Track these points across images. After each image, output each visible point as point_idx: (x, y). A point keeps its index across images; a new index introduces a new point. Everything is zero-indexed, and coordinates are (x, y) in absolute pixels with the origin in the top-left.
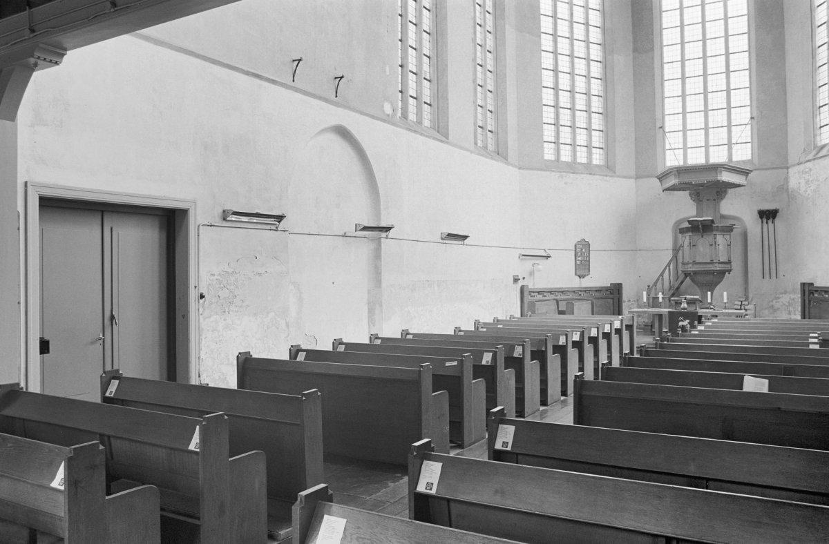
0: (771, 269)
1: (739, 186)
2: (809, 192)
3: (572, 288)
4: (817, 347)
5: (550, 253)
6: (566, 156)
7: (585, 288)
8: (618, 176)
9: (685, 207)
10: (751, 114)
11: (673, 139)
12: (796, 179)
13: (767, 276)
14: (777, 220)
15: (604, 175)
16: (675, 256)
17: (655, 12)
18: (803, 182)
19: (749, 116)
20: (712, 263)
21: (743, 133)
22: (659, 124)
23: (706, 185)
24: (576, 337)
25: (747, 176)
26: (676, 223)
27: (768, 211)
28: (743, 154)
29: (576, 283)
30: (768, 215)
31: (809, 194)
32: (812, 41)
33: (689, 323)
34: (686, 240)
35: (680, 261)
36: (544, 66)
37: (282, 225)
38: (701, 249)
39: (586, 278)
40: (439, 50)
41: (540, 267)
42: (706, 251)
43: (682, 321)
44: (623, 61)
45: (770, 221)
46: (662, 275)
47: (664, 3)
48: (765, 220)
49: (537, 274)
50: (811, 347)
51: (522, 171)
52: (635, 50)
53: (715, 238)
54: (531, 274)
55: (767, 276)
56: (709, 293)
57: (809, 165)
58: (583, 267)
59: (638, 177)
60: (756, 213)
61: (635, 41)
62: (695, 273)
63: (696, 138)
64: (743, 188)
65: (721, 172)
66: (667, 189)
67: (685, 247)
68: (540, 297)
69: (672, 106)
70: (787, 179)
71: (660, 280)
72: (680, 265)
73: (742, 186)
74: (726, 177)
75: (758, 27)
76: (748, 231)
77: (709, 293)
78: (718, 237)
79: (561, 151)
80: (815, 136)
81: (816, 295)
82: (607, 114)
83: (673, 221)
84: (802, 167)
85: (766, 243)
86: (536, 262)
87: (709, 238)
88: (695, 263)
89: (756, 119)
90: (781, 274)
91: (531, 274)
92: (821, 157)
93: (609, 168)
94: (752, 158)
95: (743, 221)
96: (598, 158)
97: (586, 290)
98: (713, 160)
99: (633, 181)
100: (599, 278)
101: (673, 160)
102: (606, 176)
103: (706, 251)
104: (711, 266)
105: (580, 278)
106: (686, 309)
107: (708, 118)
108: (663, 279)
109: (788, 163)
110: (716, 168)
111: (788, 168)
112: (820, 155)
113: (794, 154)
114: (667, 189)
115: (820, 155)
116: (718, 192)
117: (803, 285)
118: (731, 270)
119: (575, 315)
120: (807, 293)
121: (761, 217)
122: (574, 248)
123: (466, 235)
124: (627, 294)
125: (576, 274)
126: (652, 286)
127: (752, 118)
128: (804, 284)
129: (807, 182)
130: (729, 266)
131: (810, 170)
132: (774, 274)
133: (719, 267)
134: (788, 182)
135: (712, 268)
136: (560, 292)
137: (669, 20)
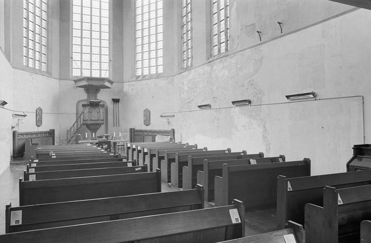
0: (117, 123)
1: (109, 88)
2: (133, 92)
3: (31, 132)
4: (55, 157)
5: (26, 114)
6: (153, 71)
7: (41, 132)
8: (53, 78)
9: (83, 95)
10: (109, 59)
11: (76, 64)
12: (127, 87)
13: (115, 126)
15: (48, 77)
17: (71, 5)
18: (130, 89)
20: (98, 120)
21: (105, 66)
22: (71, 56)
23: (93, 87)
24: (146, 150)
25: (112, 84)
26: (78, 101)
27: (116, 99)
28: (105, 75)
29: (36, 129)
30: (116, 101)
31: (133, 94)
33: (107, 146)
34: (87, 110)
38: (94, 114)
39: (41, 126)
41: (23, 121)
42: (96, 115)
43: (104, 145)
44: (56, 23)
45: (117, 104)
46: (74, 125)
47: (74, 2)
48: (115, 103)
49: (20, 124)
50: (53, 157)
51: (14, 69)
53: (100, 110)
54: (18, 125)
55: (115, 126)
56: (94, 134)
57: (133, 83)
58: (39, 122)
59: (60, 79)
60: (111, 100)
62: (91, 124)
63: (86, 65)
64: (108, 89)
68: (22, 137)
69: (76, 49)
70: (123, 87)
71: (73, 128)
73: (77, 87)
75: (114, 24)
77: (94, 134)
78: (101, 109)
80: (135, 72)
81: (136, 133)
82: (47, 47)
83: (77, 101)
84: (130, 83)
85: (115, 112)
86: (20, 118)
87: (97, 109)
88: (91, 120)
89: (112, 61)
90: (120, 125)
91: (18, 125)
93: (49, 73)
95: (105, 102)
96: (44, 68)
97: (41, 133)
98: (103, 76)
99: (58, 81)
100: (45, 127)
101: (76, 73)
102: (49, 77)
103: (96, 115)
104: (98, 121)
105: (38, 126)
106: (105, 140)
107: (91, 58)
109: (123, 81)
110: (103, 80)
111: (123, 83)
113: (126, 77)
115: (138, 80)
116: (96, 90)
117: (131, 129)
119: (56, 145)
120: (133, 132)
122: (35, 112)
123: (7, 102)
124: (56, 134)
125: (36, 125)
126: (69, 131)
128: (131, 129)
129: (132, 89)
131: (134, 85)
134: (123, 88)
135: (98, 122)
136: (25, 134)
137: (76, 10)
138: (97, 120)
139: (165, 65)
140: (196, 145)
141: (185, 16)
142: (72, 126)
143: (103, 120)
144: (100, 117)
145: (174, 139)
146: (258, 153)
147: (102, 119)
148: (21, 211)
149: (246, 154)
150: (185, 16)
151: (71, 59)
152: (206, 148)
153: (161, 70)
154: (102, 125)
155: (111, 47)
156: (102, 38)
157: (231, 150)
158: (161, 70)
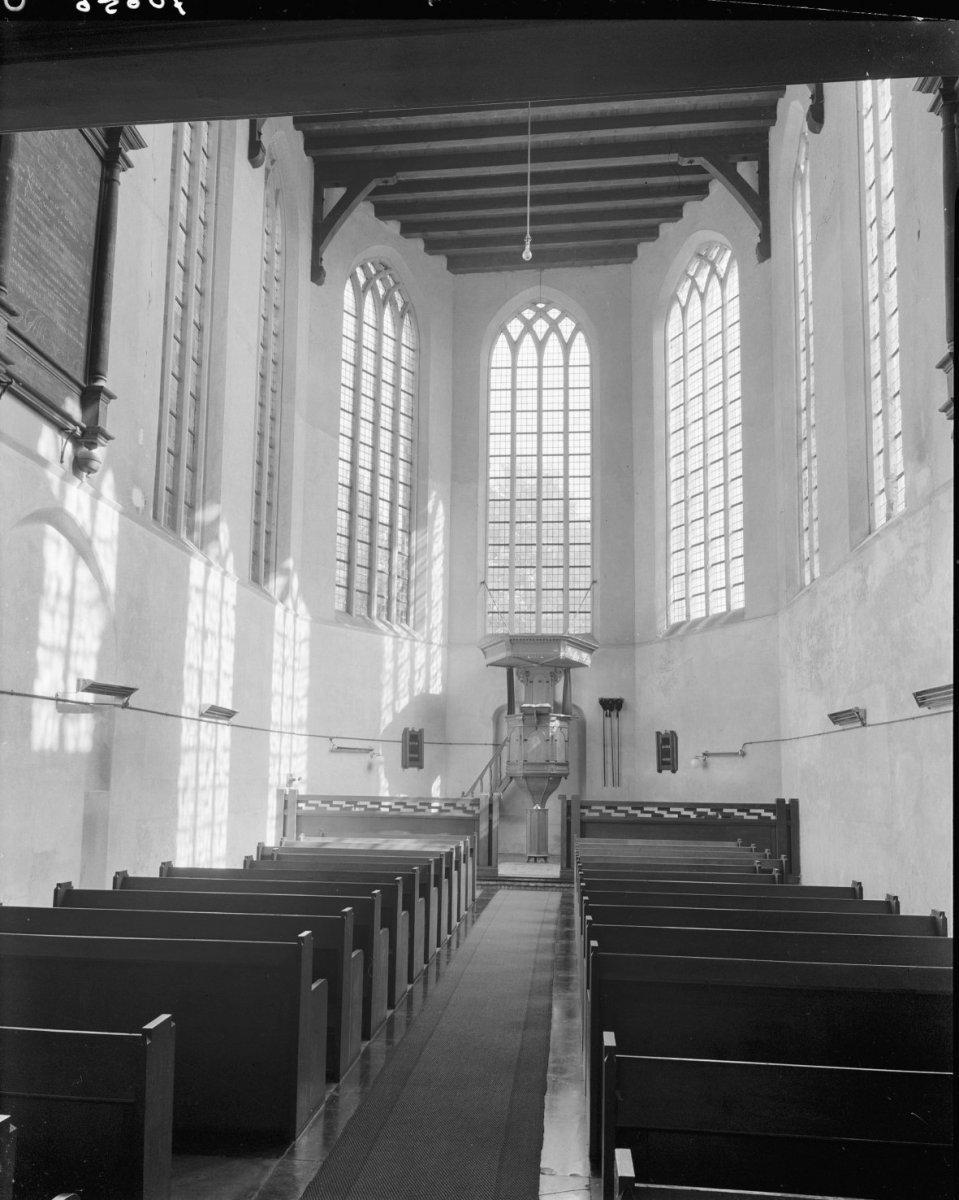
6: (718, 606)
14: (621, 713)
16: (497, 756)
19: (589, 579)
28: (579, 625)
30: (612, 706)
32: (861, 245)
35: (505, 760)
36: (341, 430)
37: (133, 700)
40: (210, 425)
45: (614, 713)
46: (481, 778)
52: (454, 478)
60: (597, 702)
61: (454, 467)
65: (565, 646)
66: (492, 664)
67: (513, 740)
72: (504, 765)
74: (571, 653)
76: (587, 725)
79: (370, 460)
92: (485, 770)
94: (593, 630)
98: (546, 631)
108: (482, 784)
110: (557, 640)
112: (488, 770)
114: (492, 664)
118: (568, 774)
121: (605, 708)
127: (594, 582)
130: (565, 768)
132: (610, 779)
133: (556, 770)
138: (544, 764)
139: (749, 583)
140: (857, 888)
141: (901, 475)
142: (477, 781)
143: (566, 764)
144: (553, 755)
145: (569, 823)
146: (928, 913)
147: (560, 758)
148: (614, 1044)
149: (898, 911)
150: (901, 475)
151: (598, 577)
152: (896, 898)
153: (739, 600)
154: (563, 778)
155: (482, 414)
156: (535, 437)
157: (898, 904)
158: (739, 600)
